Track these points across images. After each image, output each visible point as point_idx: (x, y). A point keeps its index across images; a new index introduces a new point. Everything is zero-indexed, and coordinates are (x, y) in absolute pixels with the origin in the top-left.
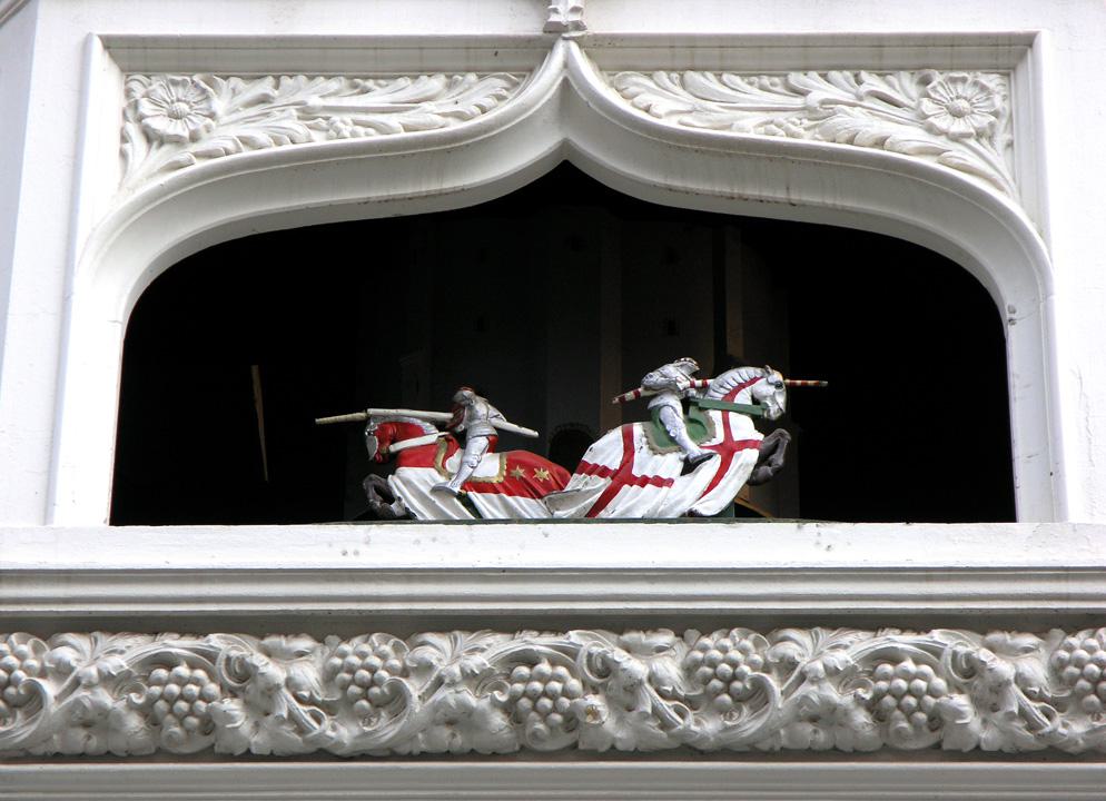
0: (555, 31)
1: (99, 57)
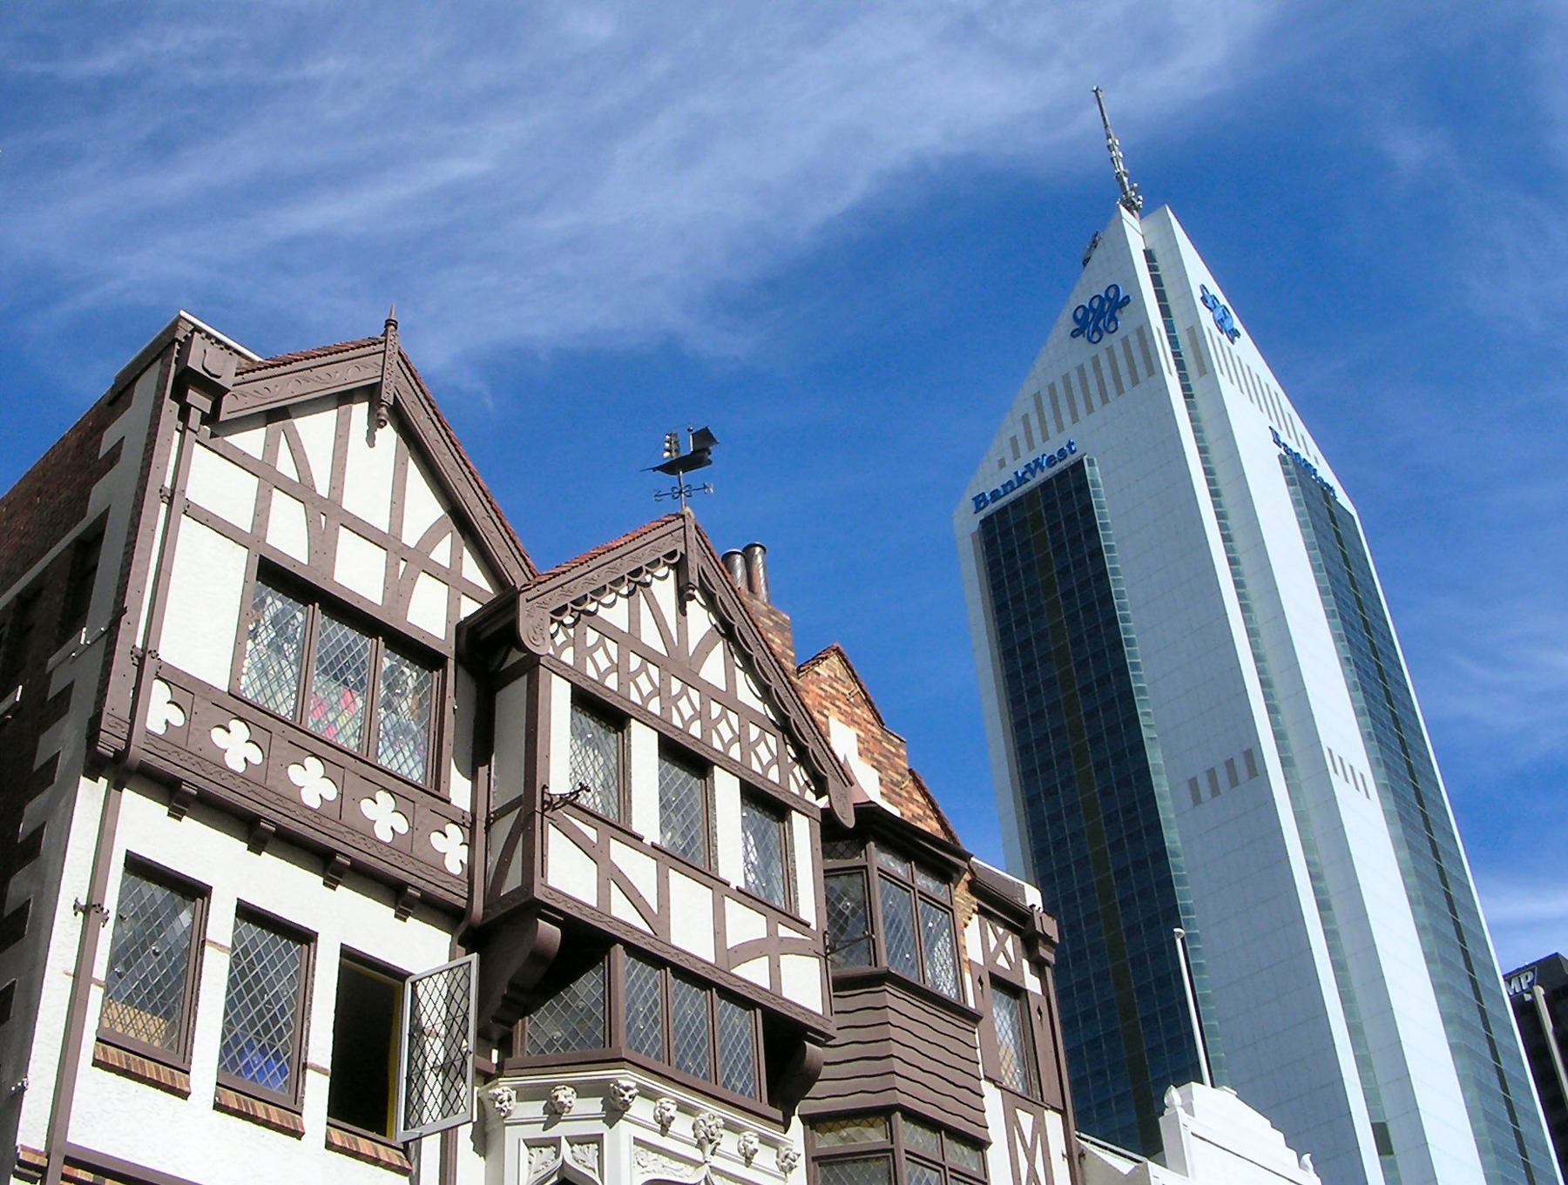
0: (706, 1162)
1: (522, 1144)
